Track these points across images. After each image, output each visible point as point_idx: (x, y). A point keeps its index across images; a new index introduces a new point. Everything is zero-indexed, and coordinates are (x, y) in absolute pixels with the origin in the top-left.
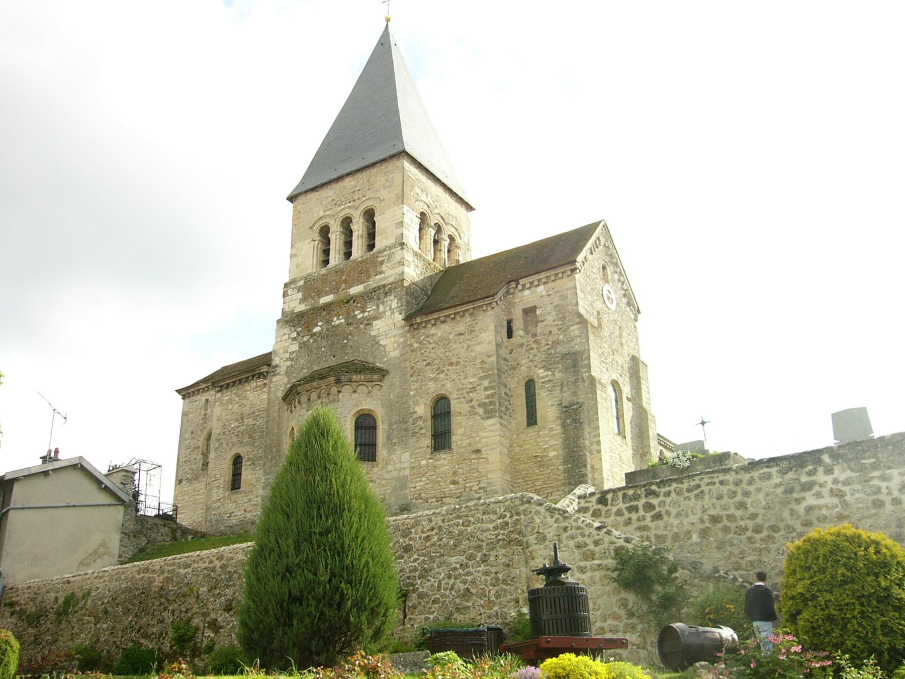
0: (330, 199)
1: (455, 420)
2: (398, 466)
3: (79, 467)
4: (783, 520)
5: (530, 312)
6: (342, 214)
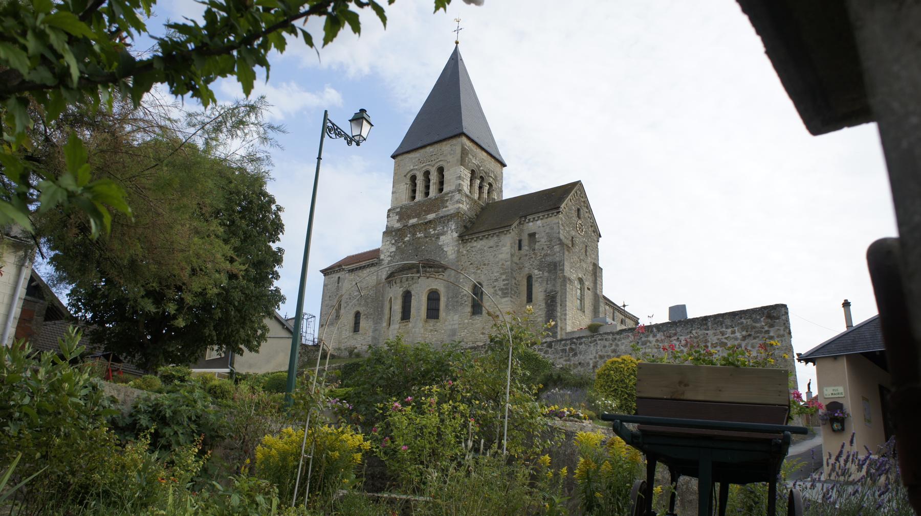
5: (532, 235)
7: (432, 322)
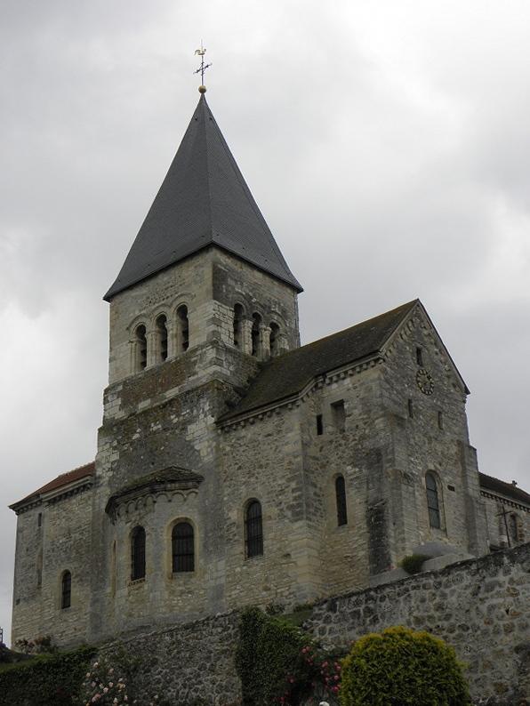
0: (145, 298)
1: (266, 524)
2: (215, 575)
4: (471, 619)
5: (338, 406)
6: (156, 313)
7: (182, 577)
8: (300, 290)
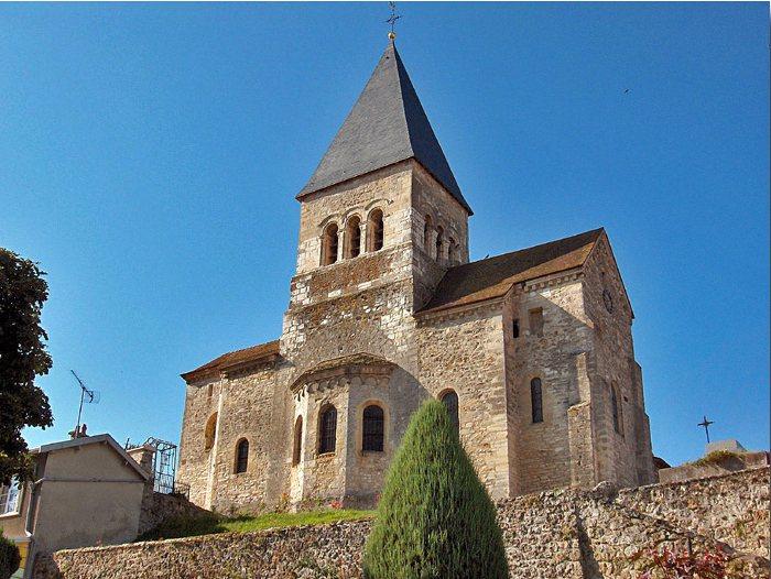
3: (105, 442)
7: (372, 456)
8: (471, 213)
